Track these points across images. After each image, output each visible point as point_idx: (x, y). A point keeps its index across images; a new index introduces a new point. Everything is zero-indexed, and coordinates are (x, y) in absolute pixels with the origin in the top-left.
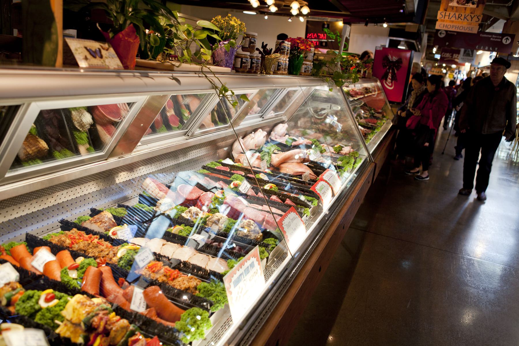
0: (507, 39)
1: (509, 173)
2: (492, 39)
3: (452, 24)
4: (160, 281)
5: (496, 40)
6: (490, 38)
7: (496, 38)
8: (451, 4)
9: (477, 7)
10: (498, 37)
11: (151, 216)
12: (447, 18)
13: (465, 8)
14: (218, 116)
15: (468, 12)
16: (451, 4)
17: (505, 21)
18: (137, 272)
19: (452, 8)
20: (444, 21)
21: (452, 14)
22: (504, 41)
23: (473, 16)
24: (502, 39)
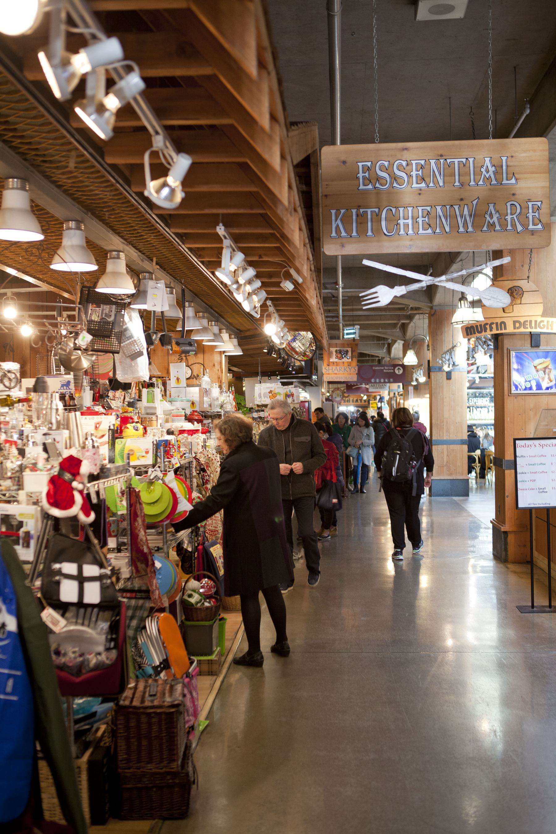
0: (399, 369)
1: (480, 523)
2: (385, 371)
3: (336, 376)
4: (231, 377)
5: (389, 371)
6: (383, 370)
7: (388, 369)
8: (331, 360)
9: (352, 360)
10: (390, 368)
11: (119, 735)
12: (330, 371)
13: (343, 362)
14: (251, 247)
15: (346, 364)
16: (331, 360)
17: (403, 342)
18: (499, 655)
19: (333, 363)
20: (329, 374)
21: (334, 367)
22: (397, 372)
23: (350, 367)
24: (394, 370)
